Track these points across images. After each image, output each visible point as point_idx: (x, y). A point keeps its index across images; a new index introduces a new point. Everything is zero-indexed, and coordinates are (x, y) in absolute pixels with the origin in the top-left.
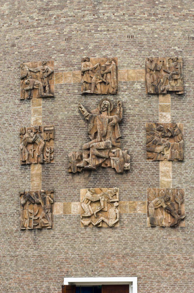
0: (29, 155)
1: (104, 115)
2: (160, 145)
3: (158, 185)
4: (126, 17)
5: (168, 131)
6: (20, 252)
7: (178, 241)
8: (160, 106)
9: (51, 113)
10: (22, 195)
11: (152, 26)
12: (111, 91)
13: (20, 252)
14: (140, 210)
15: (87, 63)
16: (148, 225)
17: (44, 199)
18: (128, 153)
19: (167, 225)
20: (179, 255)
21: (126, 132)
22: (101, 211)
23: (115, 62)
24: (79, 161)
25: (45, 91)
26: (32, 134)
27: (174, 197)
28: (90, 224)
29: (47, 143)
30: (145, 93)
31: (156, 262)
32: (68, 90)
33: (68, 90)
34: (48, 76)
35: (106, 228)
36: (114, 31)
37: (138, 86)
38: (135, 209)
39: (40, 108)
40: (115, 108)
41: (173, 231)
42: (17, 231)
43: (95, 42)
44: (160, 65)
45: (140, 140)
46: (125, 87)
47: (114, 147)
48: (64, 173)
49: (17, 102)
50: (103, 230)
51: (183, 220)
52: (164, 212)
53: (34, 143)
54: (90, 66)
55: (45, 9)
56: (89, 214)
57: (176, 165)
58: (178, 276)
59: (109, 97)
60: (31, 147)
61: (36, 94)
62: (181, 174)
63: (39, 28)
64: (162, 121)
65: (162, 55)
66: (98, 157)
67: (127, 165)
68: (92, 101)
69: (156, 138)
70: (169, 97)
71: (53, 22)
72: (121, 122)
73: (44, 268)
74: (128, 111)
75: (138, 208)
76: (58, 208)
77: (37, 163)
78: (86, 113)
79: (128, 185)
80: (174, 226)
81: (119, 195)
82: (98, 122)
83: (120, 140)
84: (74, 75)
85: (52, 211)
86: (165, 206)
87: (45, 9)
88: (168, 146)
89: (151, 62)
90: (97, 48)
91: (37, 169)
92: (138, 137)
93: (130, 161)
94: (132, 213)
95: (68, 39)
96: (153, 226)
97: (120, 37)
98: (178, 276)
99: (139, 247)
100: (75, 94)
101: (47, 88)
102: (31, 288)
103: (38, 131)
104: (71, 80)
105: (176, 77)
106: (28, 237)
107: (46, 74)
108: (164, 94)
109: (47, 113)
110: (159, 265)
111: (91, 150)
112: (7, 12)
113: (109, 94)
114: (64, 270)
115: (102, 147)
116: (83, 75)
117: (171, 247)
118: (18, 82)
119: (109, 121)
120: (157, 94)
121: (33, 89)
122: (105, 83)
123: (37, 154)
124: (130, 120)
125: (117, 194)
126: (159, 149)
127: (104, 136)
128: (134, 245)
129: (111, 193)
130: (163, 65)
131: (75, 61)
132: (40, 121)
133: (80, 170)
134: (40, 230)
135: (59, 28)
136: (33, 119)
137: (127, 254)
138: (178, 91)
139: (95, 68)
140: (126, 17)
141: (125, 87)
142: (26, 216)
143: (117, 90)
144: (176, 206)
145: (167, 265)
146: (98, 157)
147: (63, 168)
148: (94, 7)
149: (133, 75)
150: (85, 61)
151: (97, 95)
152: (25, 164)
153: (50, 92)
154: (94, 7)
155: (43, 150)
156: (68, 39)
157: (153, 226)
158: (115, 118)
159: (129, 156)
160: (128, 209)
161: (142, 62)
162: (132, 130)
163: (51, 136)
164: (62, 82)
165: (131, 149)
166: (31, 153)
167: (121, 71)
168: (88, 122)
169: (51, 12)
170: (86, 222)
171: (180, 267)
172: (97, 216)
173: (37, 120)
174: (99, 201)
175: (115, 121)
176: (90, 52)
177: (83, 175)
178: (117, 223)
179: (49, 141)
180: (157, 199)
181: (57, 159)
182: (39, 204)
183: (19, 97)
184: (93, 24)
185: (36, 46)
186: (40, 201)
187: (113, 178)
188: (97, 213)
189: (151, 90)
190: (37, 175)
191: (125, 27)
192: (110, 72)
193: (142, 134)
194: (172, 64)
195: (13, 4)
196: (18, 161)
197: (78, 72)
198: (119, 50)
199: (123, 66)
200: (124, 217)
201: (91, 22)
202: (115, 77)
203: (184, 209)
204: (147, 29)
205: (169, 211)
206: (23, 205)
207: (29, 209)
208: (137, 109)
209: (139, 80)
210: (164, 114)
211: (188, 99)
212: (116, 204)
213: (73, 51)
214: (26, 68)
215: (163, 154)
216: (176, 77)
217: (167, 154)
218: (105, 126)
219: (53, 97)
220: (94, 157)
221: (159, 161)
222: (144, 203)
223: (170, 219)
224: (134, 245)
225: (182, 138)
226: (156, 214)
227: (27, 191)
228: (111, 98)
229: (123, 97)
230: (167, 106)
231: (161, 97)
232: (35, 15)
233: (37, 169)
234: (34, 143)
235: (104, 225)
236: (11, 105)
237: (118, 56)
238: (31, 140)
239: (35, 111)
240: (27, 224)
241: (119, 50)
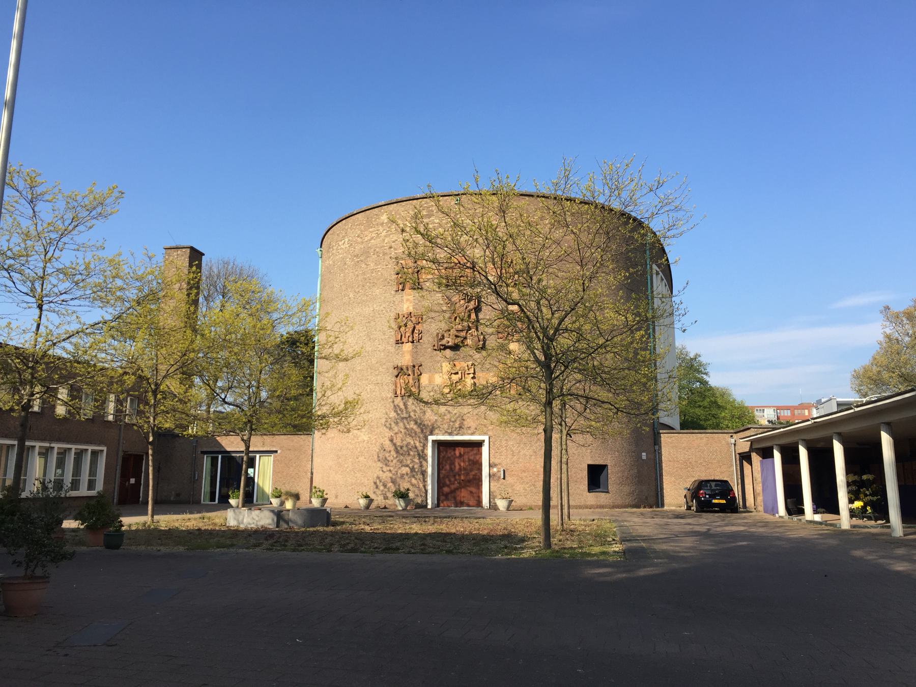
39: (411, 298)
49: (393, 293)
91: (408, 347)
123: (407, 335)
152: (399, 342)
173: (408, 307)
227: (400, 365)
233: (408, 347)
239: (408, 300)
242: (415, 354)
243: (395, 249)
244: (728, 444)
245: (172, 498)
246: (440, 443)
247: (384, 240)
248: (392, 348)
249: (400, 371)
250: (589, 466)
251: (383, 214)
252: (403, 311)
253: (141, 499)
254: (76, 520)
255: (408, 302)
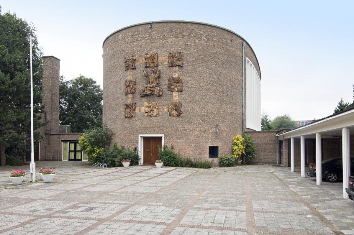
0: (127, 90)
1: (153, 74)
2: (173, 85)
3: (172, 100)
4: (162, 37)
5: (177, 80)
6: (125, 125)
7: (180, 121)
8: (174, 71)
9: (135, 75)
10: (126, 105)
11: (172, 40)
12: (155, 65)
13: (125, 125)
14: (166, 110)
15: (147, 55)
16: (168, 115)
17: (132, 106)
18: (161, 89)
19: (176, 115)
20: (180, 126)
21: (161, 81)
22: (152, 110)
23: (157, 54)
24: (144, 92)
25: (133, 66)
26: (128, 83)
27: (178, 105)
28: (148, 115)
29: (133, 86)
30: (168, 66)
31: (171, 129)
32: (141, 66)
33: (141, 66)
34: (134, 61)
35: (153, 117)
36: (157, 42)
37: (165, 63)
38: (164, 110)
39: (131, 73)
40: (156, 72)
41: (178, 118)
42: (124, 118)
43: (150, 47)
44: (174, 55)
45: (166, 84)
46: (161, 64)
47: (156, 86)
48: (139, 97)
49: (124, 71)
50: (152, 117)
51: (182, 113)
52: (174, 111)
53: (129, 86)
54: (148, 56)
55: (133, 36)
56: (147, 111)
57: (179, 93)
58: (179, 134)
59: (154, 68)
60: (128, 87)
61: (130, 68)
62: (181, 96)
63: (131, 43)
64: (174, 76)
66: (150, 90)
67: (161, 93)
68: (149, 70)
69: (172, 83)
70: (177, 67)
71: (135, 40)
72: (159, 77)
73: (132, 131)
74: (162, 73)
75: (165, 109)
76: (137, 109)
77: (130, 93)
78: (146, 74)
79: (161, 101)
80: (178, 116)
81: (158, 104)
82: (150, 77)
83: (158, 84)
84: (143, 60)
85: (135, 111)
86: (174, 108)
87: (133, 36)
88: (176, 86)
89: (171, 54)
91: (130, 96)
92: (165, 83)
93: (162, 92)
94: (163, 111)
95: (141, 47)
96: (170, 116)
97: (159, 45)
98: (179, 134)
99: (165, 123)
100: (143, 67)
101: (133, 65)
102: (128, 138)
103: (131, 81)
104: (141, 62)
105: (180, 59)
106: (128, 120)
107: (133, 60)
108: (175, 66)
109: (134, 75)
110: (172, 130)
111: (148, 88)
112: (121, 38)
113: (155, 67)
114: (139, 132)
115: (151, 87)
116: (145, 60)
117: (177, 123)
118: (124, 64)
119: (154, 77)
120: (172, 66)
121: (129, 66)
122: (153, 62)
123: (130, 90)
124: (162, 77)
125: (157, 104)
126: (173, 87)
127: (152, 82)
128: (163, 123)
129: (155, 103)
130: (175, 55)
131: (143, 55)
132: (131, 78)
133: (144, 95)
134: (131, 117)
135: (138, 42)
136: (129, 77)
137: (161, 126)
138: (181, 65)
139: (150, 57)
140: (162, 37)
141: (161, 64)
142: (127, 112)
143: (158, 65)
144: (179, 108)
145: (175, 130)
146: (150, 90)
147: (139, 95)
148: (150, 33)
149: (164, 59)
150: (146, 54)
151: (151, 67)
152: (126, 94)
153: (134, 67)
154: (150, 33)
155: (132, 88)
156: (141, 47)
157: (170, 116)
158: (156, 76)
159: (161, 90)
160: (161, 110)
161: (168, 54)
162: (163, 80)
163: (135, 83)
164: (139, 63)
165: (163, 87)
166: (128, 89)
167: (160, 58)
168: (147, 77)
169: (135, 37)
170: (146, 114)
171: (180, 131)
172: (150, 113)
173: (130, 78)
174: (150, 107)
175: (156, 76)
176: (149, 51)
177: (290, 119)
178: (157, 114)
179: (134, 85)
180: (172, 106)
181: (137, 92)
182: (131, 108)
183: (125, 70)
184: (150, 40)
185: (130, 50)
186: (131, 107)
187: (156, 98)
188: (150, 111)
189: (170, 65)
190: (130, 98)
191: (161, 41)
192: (155, 58)
193: (167, 81)
194: (179, 55)
195: (123, 35)
196: (124, 93)
197: (144, 59)
198: (159, 50)
199: (160, 56)
200: (160, 112)
201: (149, 39)
202: (157, 60)
203: (182, 109)
204: (169, 42)
205: (176, 110)
206: (126, 109)
207: (128, 110)
208: (165, 72)
209: (166, 61)
210: (175, 74)
211: (185, 68)
212: (157, 108)
213: (142, 51)
214: (127, 58)
215: (174, 89)
216: (180, 59)
217: (176, 89)
218: (153, 79)
219: (135, 69)
220: (148, 90)
221: (173, 91)
222: (167, 107)
223: (176, 113)
224: (163, 123)
225: (182, 83)
226: (171, 111)
227: (127, 103)
228: (156, 68)
229: (160, 68)
230: (177, 71)
231: (174, 68)
232: (129, 38)
233: (130, 96)
234: (129, 86)
235: (153, 116)
236: (122, 72)
237: (158, 52)
238: (128, 85)
239: (130, 74)
240: (127, 115)
241: (159, 50)
242: (133, 99)
243: (125, 51)
244: (275, 137)
245: (51, 159)
246: (146, 138)
247: (120, 47)
248: (124, 96)
249: (127, 106)
250: (210, 147)
251: (120, 35)
252: (128, 79)
253: (39, 159)
254: (335, 112)
255: (130, 76)
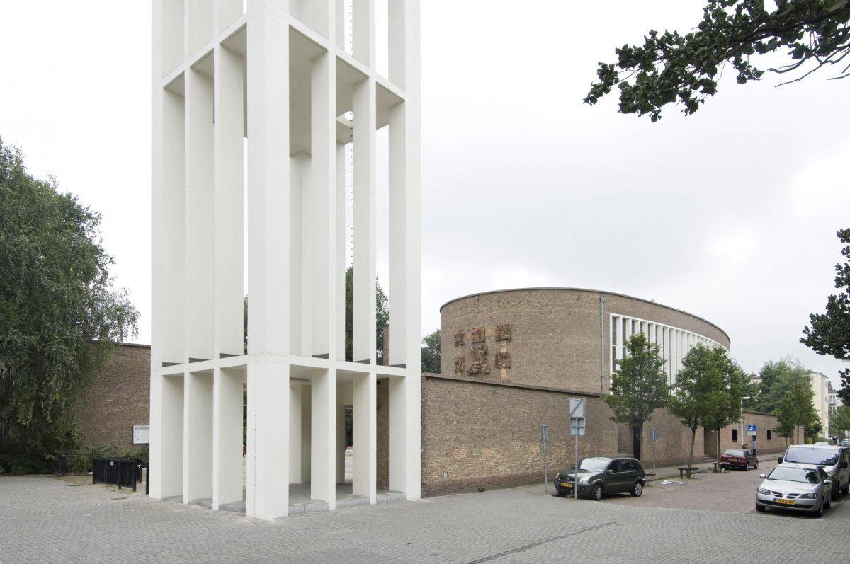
21: (488, 357)
37: (493, 338)
64: (502, 351)
65: (502, 323)
72: (486, 353)
90: (478, 324)
124: (489, 352)
126: (500, 363)
152: (456, 372)
156: (469, 321)
158: (482, 352)
167: (487, 332)
217: (504, 365)
229: (488, 342)
